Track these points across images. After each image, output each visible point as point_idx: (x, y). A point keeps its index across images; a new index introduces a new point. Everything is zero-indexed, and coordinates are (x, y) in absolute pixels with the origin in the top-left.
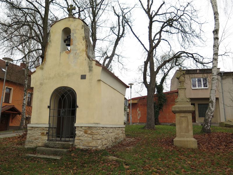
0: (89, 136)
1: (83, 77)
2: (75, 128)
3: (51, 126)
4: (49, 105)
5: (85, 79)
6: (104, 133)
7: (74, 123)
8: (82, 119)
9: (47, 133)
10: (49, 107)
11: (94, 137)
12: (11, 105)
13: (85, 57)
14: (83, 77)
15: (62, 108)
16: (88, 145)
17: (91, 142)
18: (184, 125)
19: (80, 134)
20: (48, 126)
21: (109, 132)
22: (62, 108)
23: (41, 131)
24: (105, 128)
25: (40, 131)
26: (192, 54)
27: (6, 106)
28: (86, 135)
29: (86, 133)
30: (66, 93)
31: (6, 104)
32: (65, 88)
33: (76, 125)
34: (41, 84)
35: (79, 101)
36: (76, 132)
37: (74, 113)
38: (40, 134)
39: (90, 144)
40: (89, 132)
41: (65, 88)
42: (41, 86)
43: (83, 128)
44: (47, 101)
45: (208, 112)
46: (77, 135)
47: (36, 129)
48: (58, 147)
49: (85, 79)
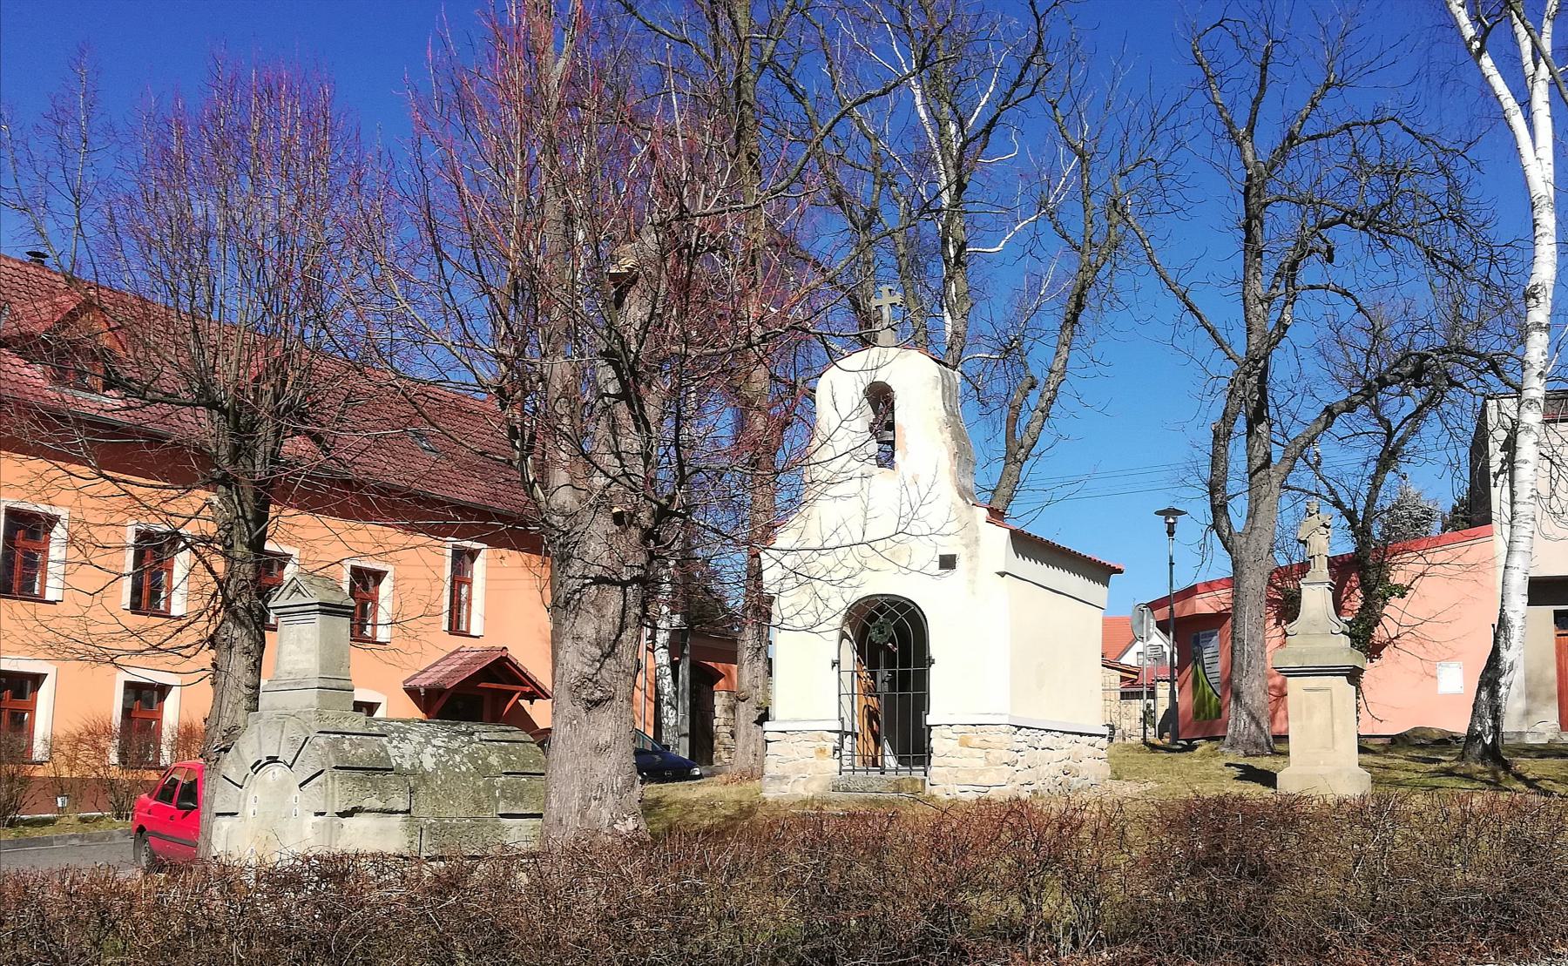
0: (978, 752)
3: (848, 728)
6: (1023, 746)
8: (950, 697)
12: (477, 645)
17: (982, 772)
18: (1319, 719)
19: (946, 750)
21: (1042, 744)
27: (457, 651)
28: (966, 751)
29: (964, 743)
30: (881, 609)
31: (458, 642)
32: (869, 600)
33: (930, 720)
35: (937, 645)
37: (920, 683)
38: (812, 752)
39: (982, 780)
40: (976, 741)
47: (796, 738)
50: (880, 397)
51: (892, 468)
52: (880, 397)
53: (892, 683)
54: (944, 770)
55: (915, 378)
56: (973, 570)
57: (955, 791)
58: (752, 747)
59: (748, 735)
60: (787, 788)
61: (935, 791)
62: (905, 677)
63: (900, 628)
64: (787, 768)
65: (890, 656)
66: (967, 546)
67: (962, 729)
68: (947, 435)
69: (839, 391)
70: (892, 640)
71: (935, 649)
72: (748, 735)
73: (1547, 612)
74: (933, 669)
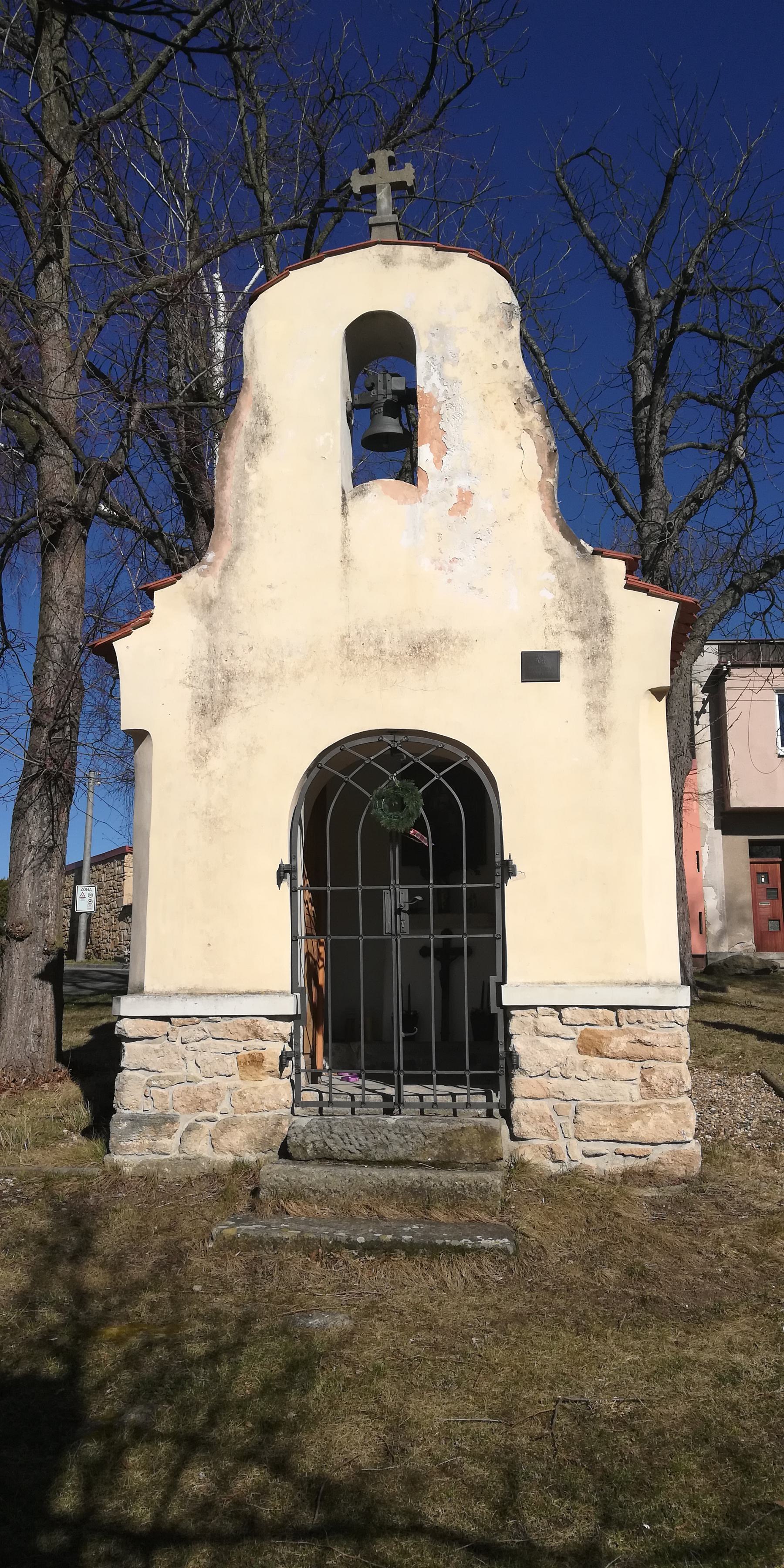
0: (622, 1067)
1: (539, 667)
2: (507, 1018)
4: (286, 861)
5: (557, 679)
7: (493, 980)
9: (284, 1059)
10: (283, 873)
11: (654, 1079)
13: (543, 524)
14: (539, 667)
15: (395, 881)
16: (617, 1135)
17: (638, 1112)
19: (547, 1061)
20: (289, 1005)
22: (395, 881)
23: (239, 1046)
24: (610, 1055)
25: (230, 1046)
26: (637, 409)
28: (597, 1064)
29: (590, 1046)
34: (204, 712)
35: (519, 832)
36: (518, 1044)
37: (487, 912)
39: (636, 1128)
40: (621, 1043)
41: (400, 738)
42: (208, 721)
43: (566, 1012)
44: (272, 836)
45: (303, 1545)
46: (524, 1063)
47: (192, 1032)
48: (401, 1153)
49: (557, 679)
50: (379, 348)
51: (414, 482)
52: (379, 348)
53: (416, 910)
54: (545, 1107)
55: (459, 307)
56: (599, 684)
57: (575, 1153)
58: (35, 1022)
59: (28, 1000)
60: (170, 1144)
61: (527, 1153)
62: (447, 904)
63: (435, 799)
64: (169, 1099)
65: (413, 855)
66: (583, 635)
67: (585, 1016)
68: (533, 416)
69: (295, 332)
70: (419, 825)
71: (515, 839)
72: (28, 1000)
73: (741, 842)
74: (512, 888)
